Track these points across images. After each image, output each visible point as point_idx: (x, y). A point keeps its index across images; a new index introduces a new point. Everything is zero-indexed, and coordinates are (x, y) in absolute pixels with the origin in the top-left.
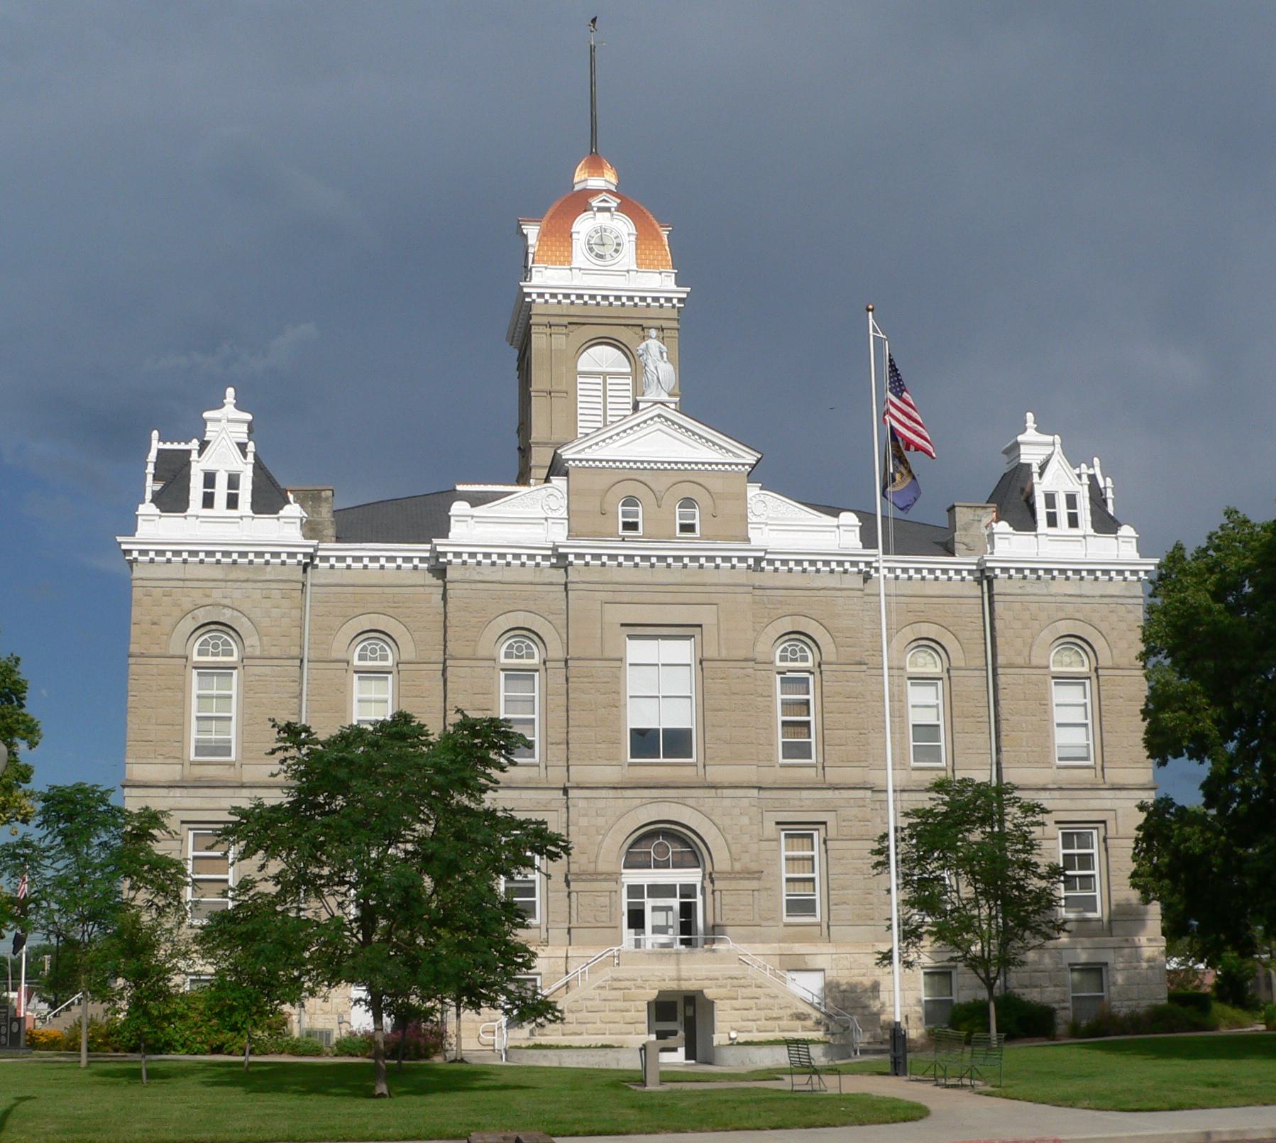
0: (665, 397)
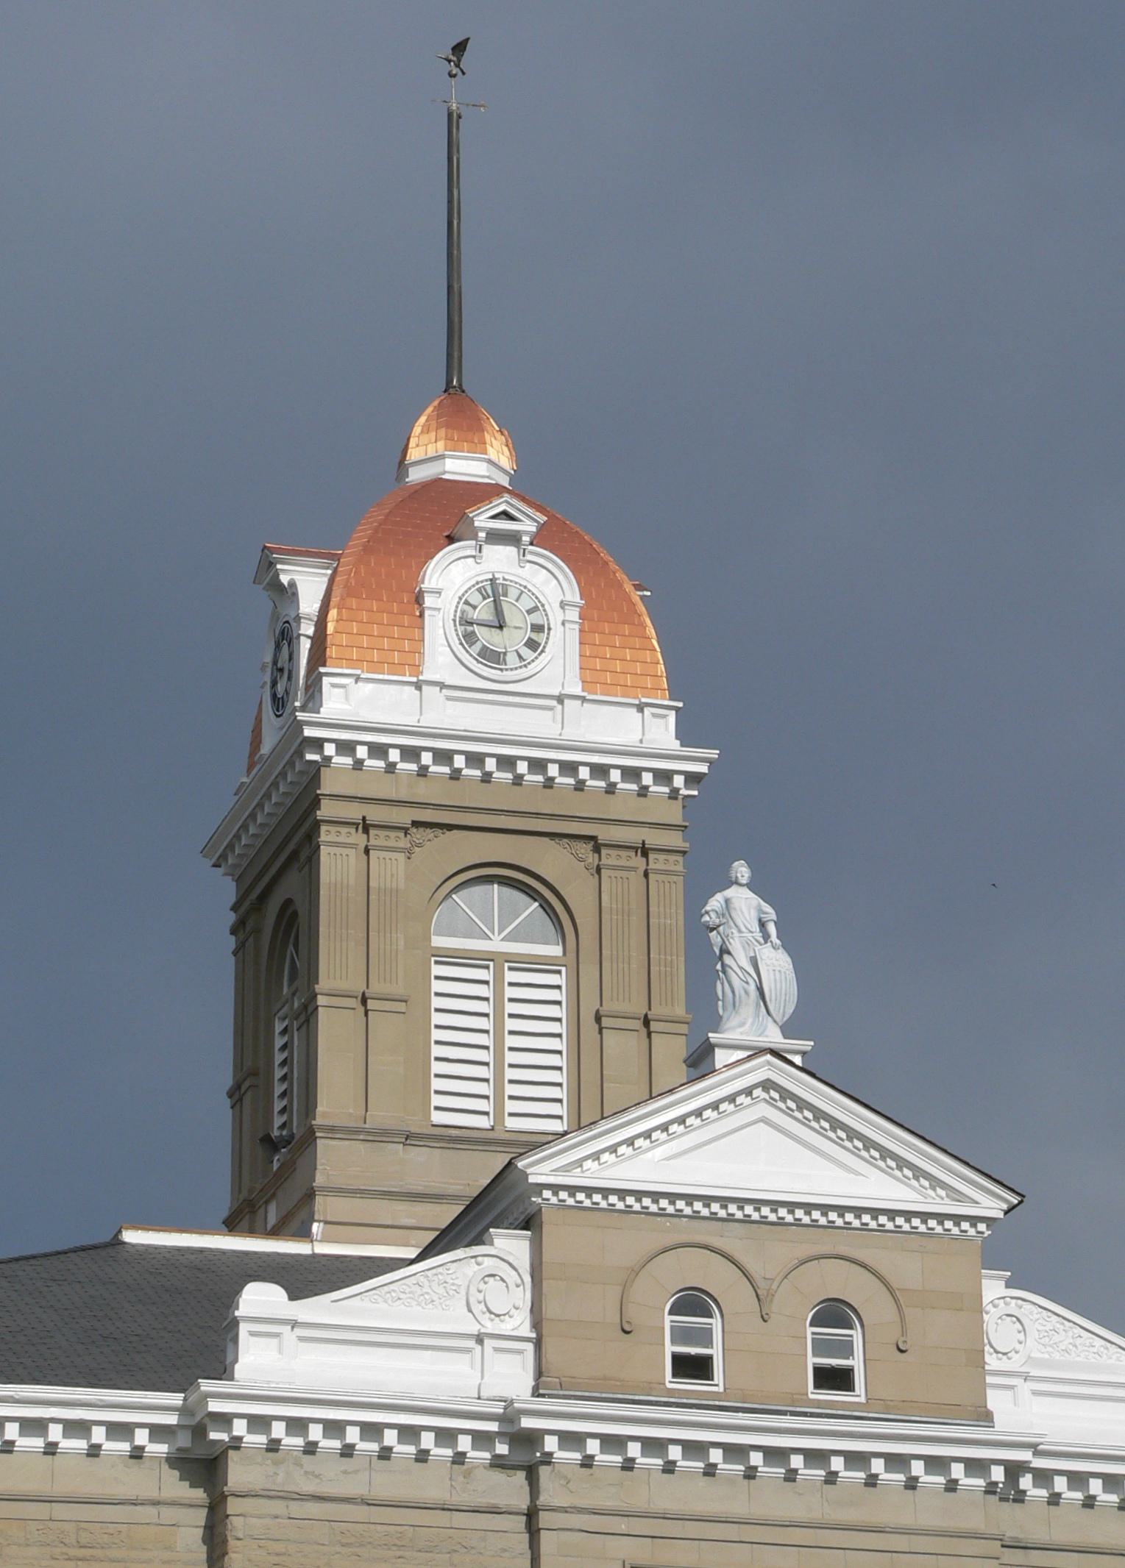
0: (774, 1037)
